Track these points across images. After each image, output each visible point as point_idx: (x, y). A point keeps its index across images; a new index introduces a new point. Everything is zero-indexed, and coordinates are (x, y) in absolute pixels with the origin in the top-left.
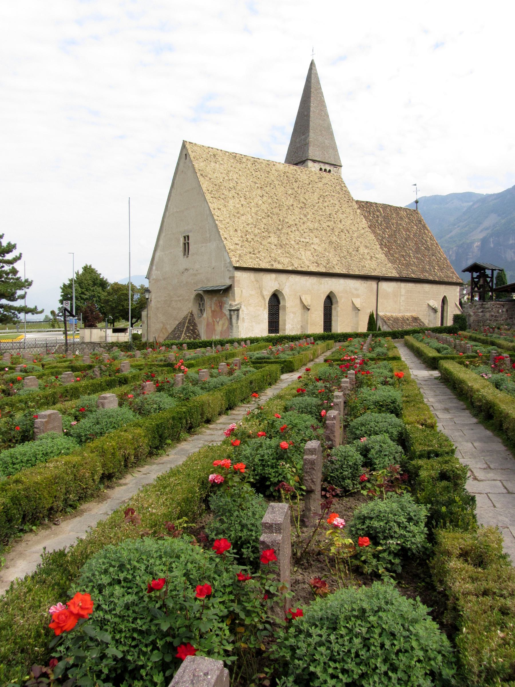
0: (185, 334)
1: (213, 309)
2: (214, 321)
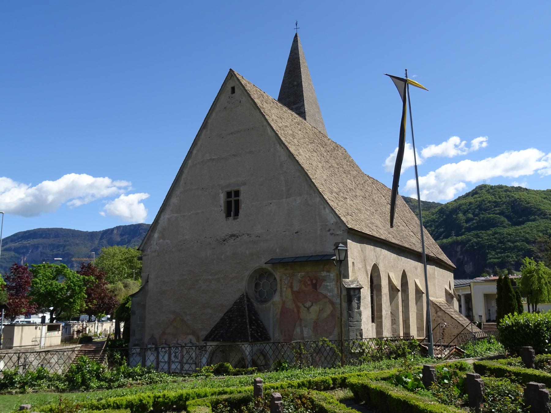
0: (251, 328)
1: (295, 289)
2: (298, 307)
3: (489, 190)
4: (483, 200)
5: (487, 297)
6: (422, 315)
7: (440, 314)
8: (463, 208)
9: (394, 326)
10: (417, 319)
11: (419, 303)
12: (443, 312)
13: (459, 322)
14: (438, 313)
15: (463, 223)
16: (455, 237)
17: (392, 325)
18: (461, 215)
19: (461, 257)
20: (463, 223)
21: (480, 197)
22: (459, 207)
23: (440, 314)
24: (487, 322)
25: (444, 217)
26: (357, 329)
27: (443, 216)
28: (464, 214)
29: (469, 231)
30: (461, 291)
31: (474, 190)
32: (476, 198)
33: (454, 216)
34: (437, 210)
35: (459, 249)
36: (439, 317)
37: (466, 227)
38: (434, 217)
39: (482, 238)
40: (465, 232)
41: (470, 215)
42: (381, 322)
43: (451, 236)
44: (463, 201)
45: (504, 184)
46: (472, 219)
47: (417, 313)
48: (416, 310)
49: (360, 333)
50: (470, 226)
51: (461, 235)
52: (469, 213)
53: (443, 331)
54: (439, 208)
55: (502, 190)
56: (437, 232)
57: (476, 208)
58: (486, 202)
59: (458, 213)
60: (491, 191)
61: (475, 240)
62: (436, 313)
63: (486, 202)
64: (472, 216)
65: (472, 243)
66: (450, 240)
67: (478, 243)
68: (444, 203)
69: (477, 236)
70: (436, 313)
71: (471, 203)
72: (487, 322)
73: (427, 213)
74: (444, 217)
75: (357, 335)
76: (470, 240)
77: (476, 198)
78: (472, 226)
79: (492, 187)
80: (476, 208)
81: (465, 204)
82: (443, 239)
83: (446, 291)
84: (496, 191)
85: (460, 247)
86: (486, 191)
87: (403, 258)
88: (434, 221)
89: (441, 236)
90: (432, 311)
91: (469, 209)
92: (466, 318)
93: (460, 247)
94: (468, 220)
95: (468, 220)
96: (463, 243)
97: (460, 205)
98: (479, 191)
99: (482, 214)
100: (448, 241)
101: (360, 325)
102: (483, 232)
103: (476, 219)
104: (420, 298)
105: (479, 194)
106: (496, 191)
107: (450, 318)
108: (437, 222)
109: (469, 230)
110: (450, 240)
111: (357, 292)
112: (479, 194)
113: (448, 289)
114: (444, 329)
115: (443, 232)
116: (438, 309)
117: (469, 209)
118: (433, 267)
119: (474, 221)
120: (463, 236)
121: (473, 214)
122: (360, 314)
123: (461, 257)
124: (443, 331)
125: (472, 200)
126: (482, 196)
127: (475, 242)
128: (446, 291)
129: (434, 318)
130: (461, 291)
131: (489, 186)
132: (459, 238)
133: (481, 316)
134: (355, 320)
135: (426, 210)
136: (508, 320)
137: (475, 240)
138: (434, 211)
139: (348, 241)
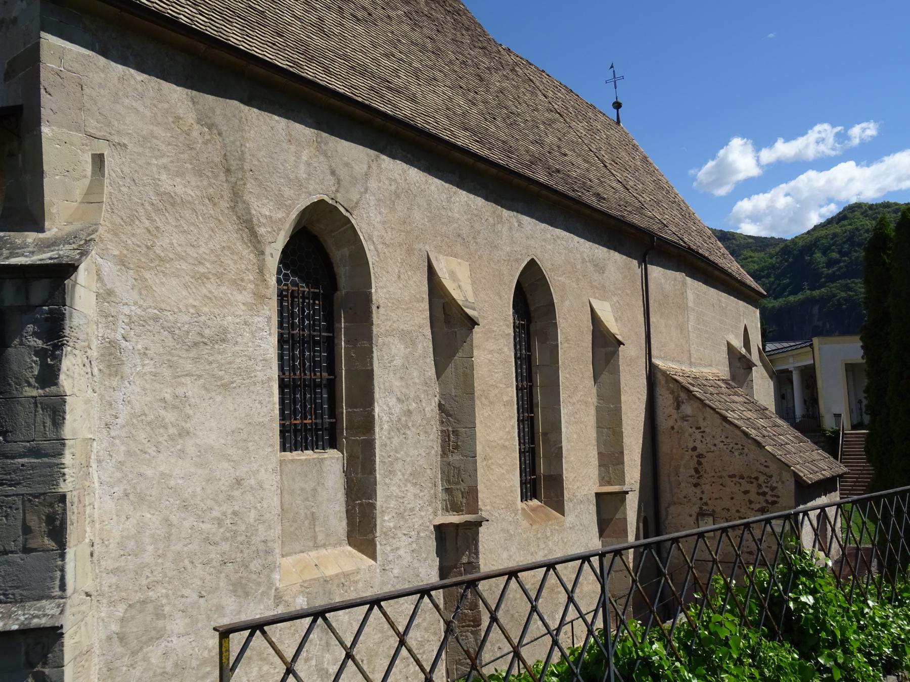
3: (866, 211)
4: (857, 229)
5: (850, 368)
6: (616, 415)
7: (688, 409)
8: (823, 244)
9: (455, 458)
10: (599, 427)
11: (605, 376)
12: (696, 404)
13: (746, 434)
14: (683, 407)
15: (823, 267)
16: (808, 292)
17: (444, 454)
18: (818, 256)
19: (820, 324)
20: (823, 267)
21: (850, 224)
22: (816, 243)
23: (688, 409)
24: (854, 427)
25: (791, 260)
26: (28, 500)
27: (789, 258)
28: (824, 253)
29: (833, 281)
30: (791, 360)
31: (840, 213)
32: (845, 226)
33: (807, 258)
34: (778, 249)
35: (816, 310)
36: (684, 418)
37: (828, 274)
38: (774, 260)
39: (855, 291)
40: (825, 282)
41: (835, 255)
42: (369, 446)
43: (802, 290)
44: (823, 233)
45: (892, 201)
46: (838, 261)
47: (598, 409)
48: (593, 399)
49: (50, 519)
50: (834, 272)
51: (819, 288)
52: (833, 251)
53: (699, 463)
54: (782, 245)
55: (890, 210)
56: (779, 285)
57: (844, 243)
58: (862, 232)
59: (814, 253)
60: (870, 212)
61: (843, 294)
62: (678, 407)
63: (862, 232)
64: (838, 256)
65: (838, 300)
66: (800, 296)
67: (848, 300)
68: (789, 238)
69: (847, 288)
70: (678, 407)
71: (835, 235)
72: (854, 427)
73: (762, 254)
74: (791, 260)
75: (27, 530)
76: (834, 296)
77: (845, 226)
78: (837, 273)
79: (871, 207)
80: (844, 243)
81: (826, 237)
82: (789, 295)
83: (730, 348)
84: (879, 213)
85: (817, 307)
86: (862, 214)
87: (526, 219)
88: (773, 267)
89: (784, 291)
90: (665, 400)
91: (833, 245)
92: (779, 421)
93: (817, 307)
94: (830, 263)
95: (830, 263)
96: (821, 301)
97: (818, 239)
98: (850, 215)
99: (856, 251)
100: (796, 300)
101: (56, 473)
102: (856, 281)
103: (844, 261)
104: (608, 362)
105: (850, 219)
106: (879, 213)
107: (718, 420)
108: (778, 268)
109: (832, 278)
110: (800, 296)
111: (39, 291)
112: (850, 219)
113: (738, 343)
114: (700, 456)
115: (788, 285)
116: (683, 396)
117: (833, 245)
118: (679, 276)
119: (842, 264)
120: (823, 290)
121: (840, 252)
122: (56, 411)
123: (820, 324)
124: (699, 463)
125: (838, 230)
126: (855, 222)
127: (843, 298)
128: (730, 348)
129: (671, 423)
130: (791, 360)
131: (866, 204)
132: (816, 293)
133: (838, 416)
134: (20, 447)
135: (759, 251)
136: (334, 420)
137: (843, 294)
138: (772, 251)
139: (50, 42)
